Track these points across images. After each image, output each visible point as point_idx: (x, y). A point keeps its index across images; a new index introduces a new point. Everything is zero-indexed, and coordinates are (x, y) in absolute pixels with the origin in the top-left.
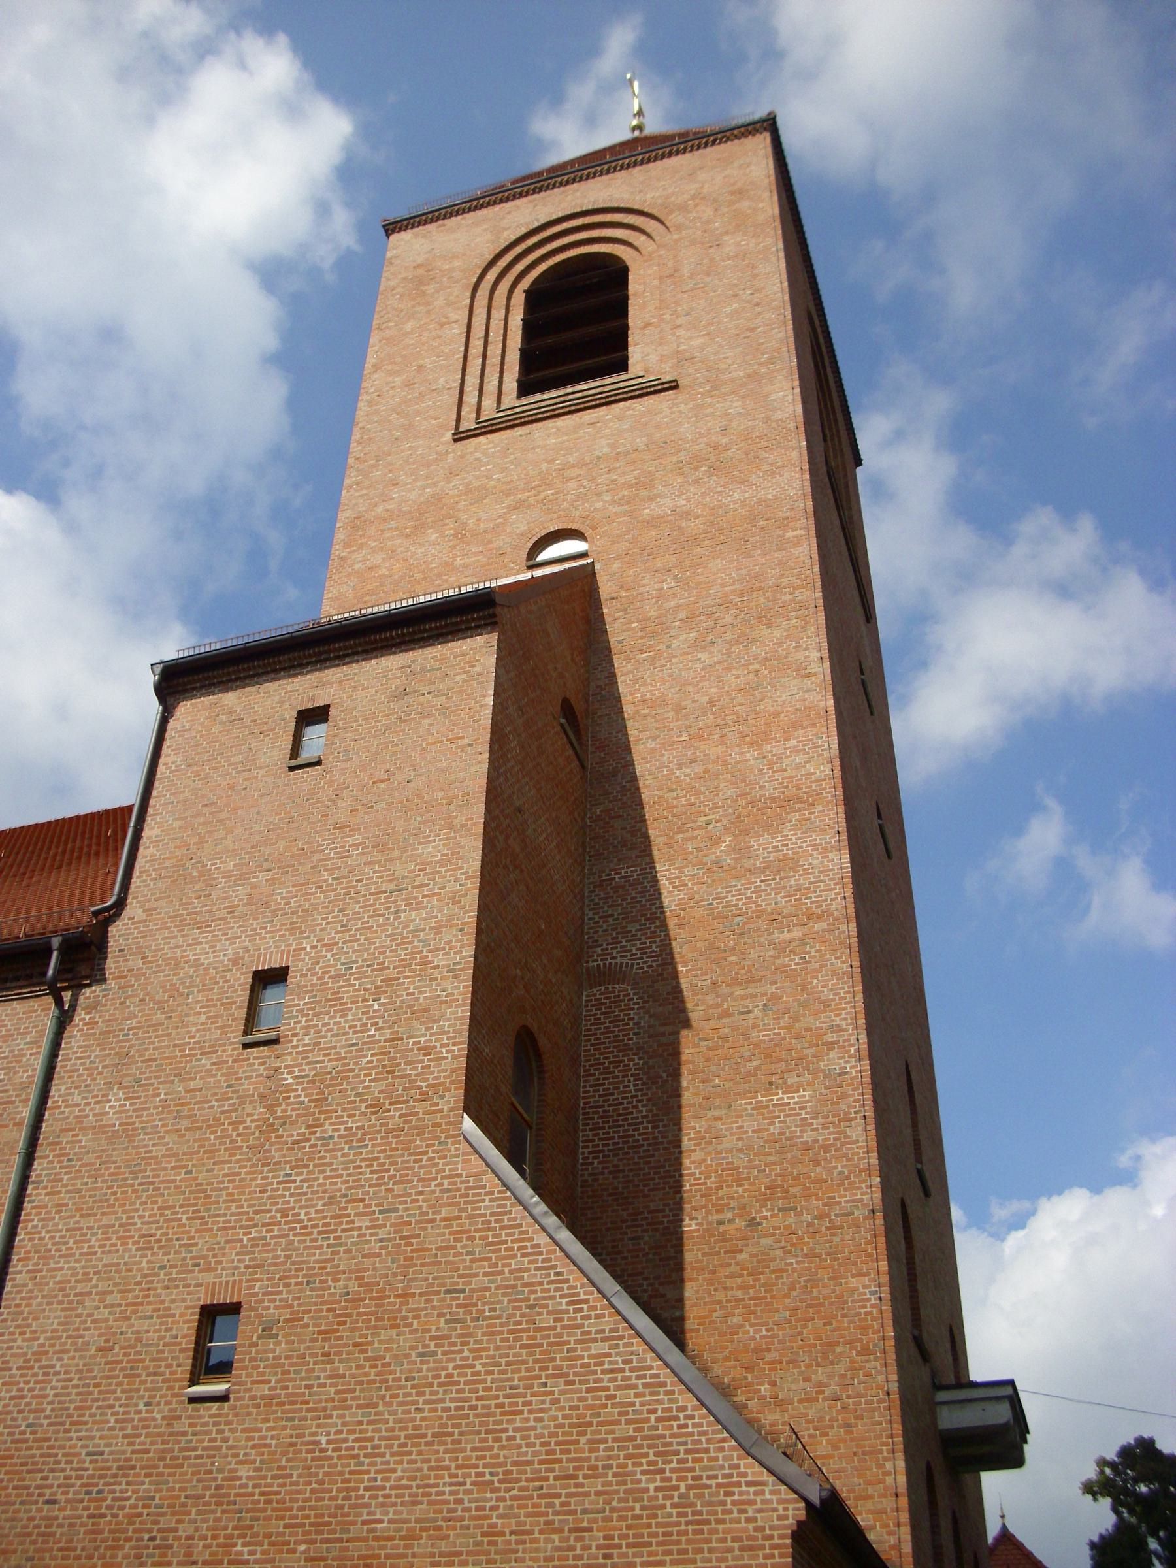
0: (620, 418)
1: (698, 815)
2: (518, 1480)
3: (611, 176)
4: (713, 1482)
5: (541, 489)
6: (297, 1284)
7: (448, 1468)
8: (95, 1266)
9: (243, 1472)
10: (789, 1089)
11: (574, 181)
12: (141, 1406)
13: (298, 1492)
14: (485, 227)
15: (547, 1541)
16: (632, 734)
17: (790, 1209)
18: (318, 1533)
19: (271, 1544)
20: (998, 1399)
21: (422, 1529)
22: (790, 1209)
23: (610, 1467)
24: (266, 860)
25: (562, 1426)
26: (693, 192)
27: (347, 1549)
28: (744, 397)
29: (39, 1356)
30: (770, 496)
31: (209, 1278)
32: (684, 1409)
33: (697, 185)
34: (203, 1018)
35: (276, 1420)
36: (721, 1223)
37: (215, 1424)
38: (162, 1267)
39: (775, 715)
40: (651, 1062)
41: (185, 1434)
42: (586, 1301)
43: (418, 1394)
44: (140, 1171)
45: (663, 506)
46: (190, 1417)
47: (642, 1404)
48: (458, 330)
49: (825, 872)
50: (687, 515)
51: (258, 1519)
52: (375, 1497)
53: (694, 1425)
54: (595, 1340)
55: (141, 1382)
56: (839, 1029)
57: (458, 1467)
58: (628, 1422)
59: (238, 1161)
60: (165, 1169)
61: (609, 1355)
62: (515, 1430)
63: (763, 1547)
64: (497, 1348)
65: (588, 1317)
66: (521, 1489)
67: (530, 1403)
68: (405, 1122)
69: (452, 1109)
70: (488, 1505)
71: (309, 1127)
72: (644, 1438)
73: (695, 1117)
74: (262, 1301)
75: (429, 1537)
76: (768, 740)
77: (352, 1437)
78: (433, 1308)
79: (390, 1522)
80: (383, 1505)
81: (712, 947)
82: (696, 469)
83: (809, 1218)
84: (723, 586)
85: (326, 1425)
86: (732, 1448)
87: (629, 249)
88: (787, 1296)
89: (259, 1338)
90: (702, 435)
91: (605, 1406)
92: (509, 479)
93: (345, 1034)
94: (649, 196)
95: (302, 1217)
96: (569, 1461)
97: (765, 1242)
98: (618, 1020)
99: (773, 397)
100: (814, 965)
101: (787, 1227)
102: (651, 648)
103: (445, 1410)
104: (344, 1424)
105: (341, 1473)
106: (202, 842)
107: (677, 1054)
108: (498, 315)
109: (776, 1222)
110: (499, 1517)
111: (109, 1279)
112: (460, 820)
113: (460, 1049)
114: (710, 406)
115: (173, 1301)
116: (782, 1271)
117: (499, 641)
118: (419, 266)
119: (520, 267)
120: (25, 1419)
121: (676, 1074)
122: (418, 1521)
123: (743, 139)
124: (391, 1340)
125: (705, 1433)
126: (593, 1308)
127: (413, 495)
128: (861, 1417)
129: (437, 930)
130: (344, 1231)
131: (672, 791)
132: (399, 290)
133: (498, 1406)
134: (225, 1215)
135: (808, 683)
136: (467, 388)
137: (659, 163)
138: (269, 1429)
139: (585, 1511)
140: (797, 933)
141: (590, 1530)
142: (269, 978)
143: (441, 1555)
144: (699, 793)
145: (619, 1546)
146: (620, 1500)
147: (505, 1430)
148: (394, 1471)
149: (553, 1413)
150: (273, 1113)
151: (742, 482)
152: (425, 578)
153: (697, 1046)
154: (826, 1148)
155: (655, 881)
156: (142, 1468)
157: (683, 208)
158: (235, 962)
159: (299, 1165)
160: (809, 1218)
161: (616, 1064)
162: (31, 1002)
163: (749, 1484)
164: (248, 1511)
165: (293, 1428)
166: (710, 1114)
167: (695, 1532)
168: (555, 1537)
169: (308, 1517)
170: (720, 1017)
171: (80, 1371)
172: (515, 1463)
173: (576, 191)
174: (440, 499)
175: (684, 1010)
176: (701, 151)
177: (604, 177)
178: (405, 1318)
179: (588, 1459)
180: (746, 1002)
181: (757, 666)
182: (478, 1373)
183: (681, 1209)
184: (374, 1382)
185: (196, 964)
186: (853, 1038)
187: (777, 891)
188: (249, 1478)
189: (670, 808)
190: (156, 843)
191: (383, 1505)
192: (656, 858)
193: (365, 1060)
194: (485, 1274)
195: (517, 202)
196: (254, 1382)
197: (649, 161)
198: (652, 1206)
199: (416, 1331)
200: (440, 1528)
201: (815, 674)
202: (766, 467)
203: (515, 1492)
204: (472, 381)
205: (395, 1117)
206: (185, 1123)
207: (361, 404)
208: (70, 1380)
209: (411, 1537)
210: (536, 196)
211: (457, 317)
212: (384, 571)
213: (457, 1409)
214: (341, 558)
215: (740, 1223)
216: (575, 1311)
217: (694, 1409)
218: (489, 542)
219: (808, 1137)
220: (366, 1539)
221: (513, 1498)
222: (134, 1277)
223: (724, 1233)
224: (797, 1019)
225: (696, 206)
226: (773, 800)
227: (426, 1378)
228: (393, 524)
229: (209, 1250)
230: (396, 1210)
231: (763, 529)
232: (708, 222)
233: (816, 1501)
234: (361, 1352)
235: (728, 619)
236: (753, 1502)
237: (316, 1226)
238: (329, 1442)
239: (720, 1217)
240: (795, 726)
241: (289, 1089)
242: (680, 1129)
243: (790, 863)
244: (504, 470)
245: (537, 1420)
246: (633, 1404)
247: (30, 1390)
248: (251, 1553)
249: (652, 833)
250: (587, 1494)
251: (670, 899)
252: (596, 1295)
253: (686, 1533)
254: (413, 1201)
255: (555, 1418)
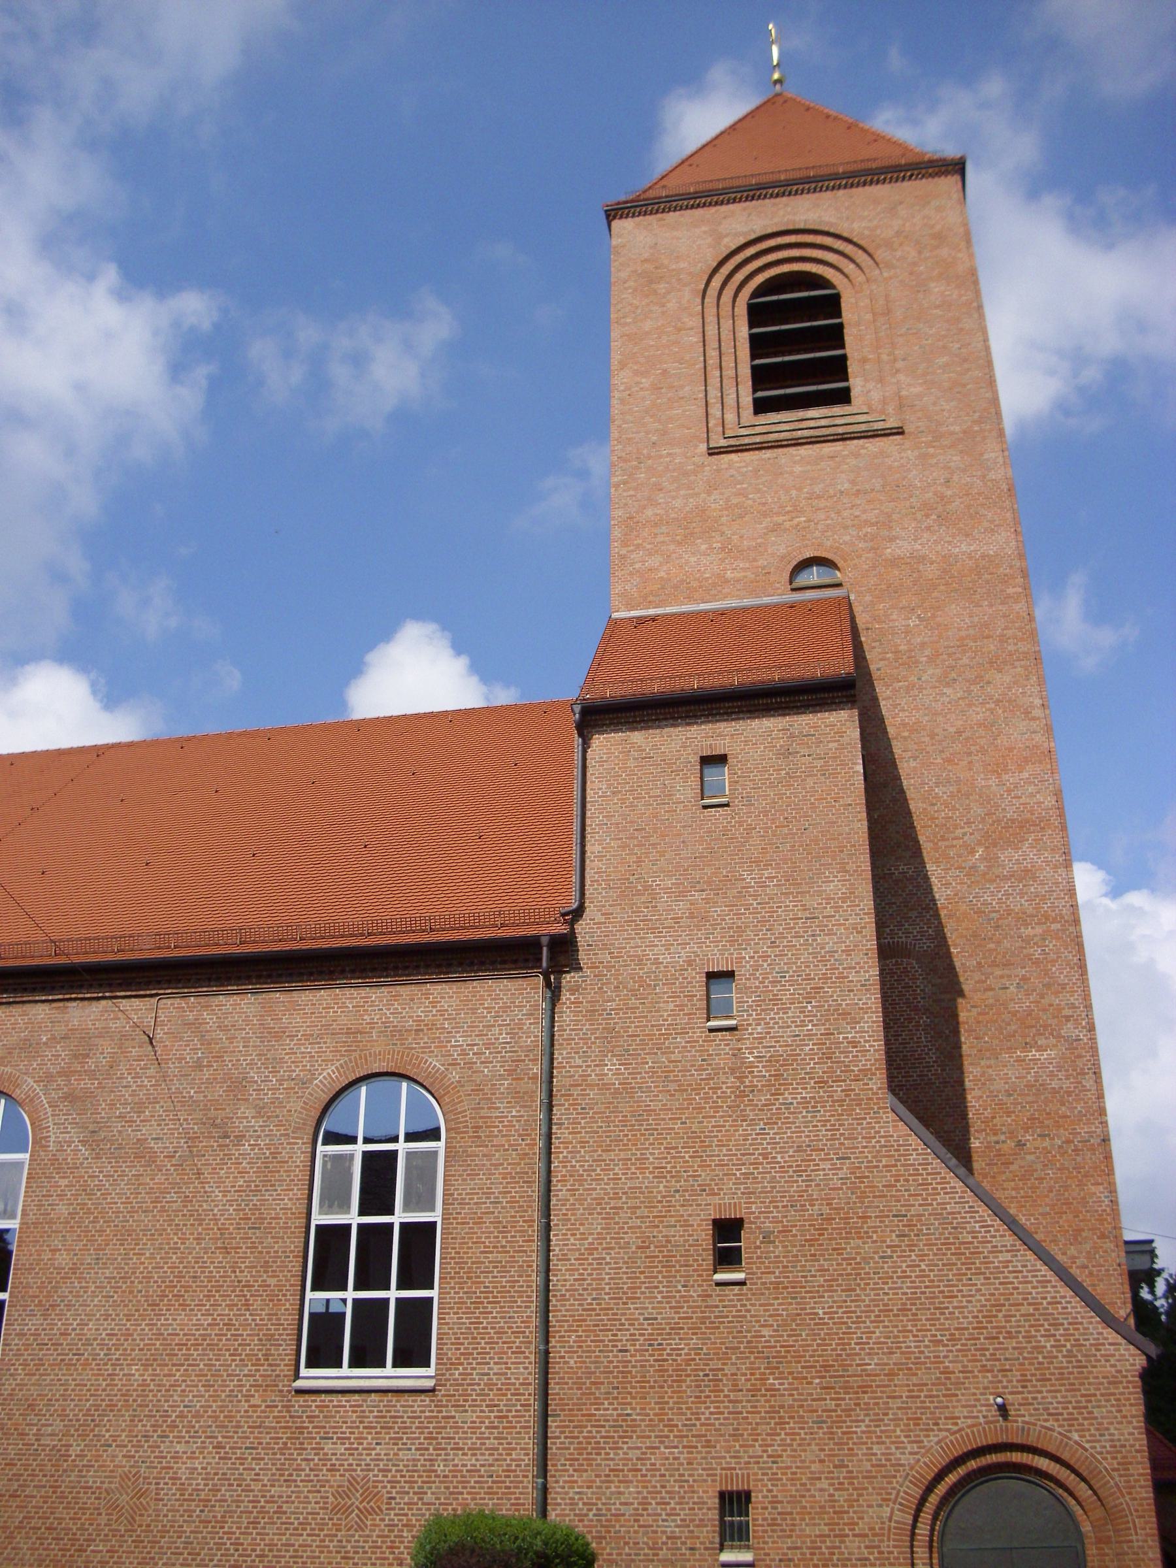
0: (857, 455)
1: (956, 827)
2: (960, 1339)
3: (817, 195)
4: (1087, 1343)
5: (794, 515)
6: (783, 1207)
7: (911, 1331)
8: (622, 1188)
9: (766, 1332)
10: (1040, 1049)
11: (783, 195)
12: (680, 1288)
13: (808, 1345)
14: (704, 228)
15: (984, 1377)
16: (897, 750)
17: (1045, 1136)
18: (827, 1371)
19: (794, 1378)
20: (1143, 1252)
21: (899, 1370)
22: (1045, 1136)
23: (1020, 1332)
24: (699, 882)
25: (985, 1306)
26: (896, 228)
27: (848, 1382)
28: (961, 452)
29: (591, 1250)
30: (991, 552)
31: (716, 1200)
32: (1065, 1297)
33: (900, 222)
34: (671, 1006)
35: (783, 1298)
36: (997, 1142)
37: (739, 1300)
38: (678, 1191)
39: (1011, 749)
40: (936, 1020)
41: (717, 1307)
42: (993, 1226)
43: (884, 1283)
44: (644, 1120)
45: (901, 548)
46: (718, 1295)
47: (1037, 1293)
48: (696, 339)
49: (1057, 883)
50: (923, 559)
51: (781, 1362)
52: (863, 1349)
53: (1073, 1308)
54: (1001, 1252)
55: (677, 1271)
56: (1073, 1006)
57: (918, 1331)
58: (1029, 1304)
59: (722, 1117)
60: (664, 1119)
61: (1011, 1261)
62: (955, 1308)
63: (1121, 1382)
64: (935, 1255)
65: (995, 1237)
66: (963, 1345)
67: (961, 1291)
68: (846, 1096)
69: (880, 1089)
70: (942, 1354)
71: (772, 1095)
72: (1041, 1315)
73: (971, 1064)
74: (759, 1218)
75: (904, 1374)
76: (1006, 771)
77: (841, 1310)
78: (886, 1226)
79: (876, 1364)
80: (869, 1354)
81: (975, 936)
82: (927, 516)
83: (1060, 1143)
84: (959, 629)
85: (821, 1302)
86: (1098, 1323)
87: (838, 274)
88: (1047, 1196)
89: (762, 1242)
90: (929, 485)
91: (1012, 1294)
92: (764, 500)
93: (789, 1027)
94: (855, 225)
95: (779, 1159)
96: (992, 1328)
97: (1030, 1158)
98: (907, 987)
99: (986, 456)
100: (1053, 956)
101: (1044, 1148)
102: (905, 679)
103: (904, 1294)
104: (834, 1302)
105: (837, 1334)
106: (639, 861)
107: (955, 1016)
108: (727, 324)
109: (1038, 1143)
110: (950, 1362)
111: (636, 1198)
112: (851, 867)
113: (879, 1045)
114: (932, 456)
115: (690, 1215)
116: (1043, 1179)
117: (860, 715)
118: (646, 261)
119: (740, 276)
120: (589, 1294)
121: (956, 1032)
122: (895, 1364)
123: (936, 179)
124: (858, 1247)
125: (1079, 1313)
126: (998, 1231)
127: (678, 503)
128: (1101, 1280)
129: (847, 952)
130: (812, 1171)
131: (933, 805)
132: (631, 283)
133: (940, 1292)
134: (718, 1156)
135: (1034, 725)
136: (711, 401)
137: (860, 189)
138: (779, 1304)
139: (1006, 1359)
140: (1039, 930)
141: (1011, 1370)
142: (719, 977)
143: (914, 1385)
144: (954, 809)
145: (1031, 1381)
146: (1029, 1353)
147: (947, 1308)
148: (874, 1332)
149: (978, 1297)
150: (742, 1082)
151: (967, 535)
152: (700, 587)
153: (970, 1011)
154: (1069, 1093)
155: (926, 878)
156: (689, 1329)
157: (888, 244)
158: (690, 963)
159: (770, 1123)
160: (1060, 1143)
161: (910, 1020)
162: (520, 982)
163: (1110, 1344)
164: (774, 1357)
165: (797, 1304)
166: (983, 1063)
167: (1079, 1373)
168: (989, 1375)
169: (818, 1361)
170: (986, 990)
171: (627, 1263)
172: (957, 1329)
173: (786, 205)
174: (703, 511)
175: (958, 983)
176: (898, 184)
177: (810, 196)
178: (867, 1232)
179: (1004, 1327)
180: (1004, 981)
181: (993, 706)
182: (924, 1271)
183: (968, 1132)
184: (851, 1274)
185: (657, 962)
186: (1084, 1015)
187: (1022, 895)
188: (771, 1336)
189: (933, 819)
190: (600, 858)
191: (869, 1354)
192: (926, 860)
193: (807, 1048)
194: (920, 1205)
195: (731, 206)
196: (762, 1273)
197: (852, 186)
198: (946, 1128)
199: (876, 1242)
200: (910, 1369)
201: (1038, 718)
202: (986, 524)
203: (959, 1347)
204: (714, 394)
205: (838, 1089)
206: (672, 1087)
207: (614, 402)
208: (620, 1268)
209: (891, 1374)
210: (748, 203)
211: (690, 324)
212: (662, 574)
213: (912, 1293)
214: (623, 557)
215: (1011, 1144)
216: (986, 1232)
217: (1071, 1297)
218: (755, 560)
219: (1055, 1084)
220: (861, 1376)
221: (958, 1351)
222: (656, 1197)
223: (999, 1150)
224: (1042, 996)
225: (901, 244)
226: (1013, 821)
227: (887, 1273)
228: (664, 529)
229: (712, 1180)
230: (849, 1158)
231: (987, 582)
232: (915, 264)
233: (1154, 1356)
234: (838, 1254)
235: (965, 661)
236: (1114, 1355)
237: (791, 1166)
238: (825, 1313)
239: (995, 1138)
240: (1026, 760)
241: (751, 1065)
242: (963, 1073)
243: (1028, 874)
244: (759, 491)
245: (968, 1302)
246: (1030, 1293)
247: (589, 1275)
248: (780, 1384)
249: (922, 839)
250: (1007, 1349)
251: (941, 894)
252: (999, 1222)
253: (1072, 1373)
254: (861, 1152)
255: (980, 1301)
